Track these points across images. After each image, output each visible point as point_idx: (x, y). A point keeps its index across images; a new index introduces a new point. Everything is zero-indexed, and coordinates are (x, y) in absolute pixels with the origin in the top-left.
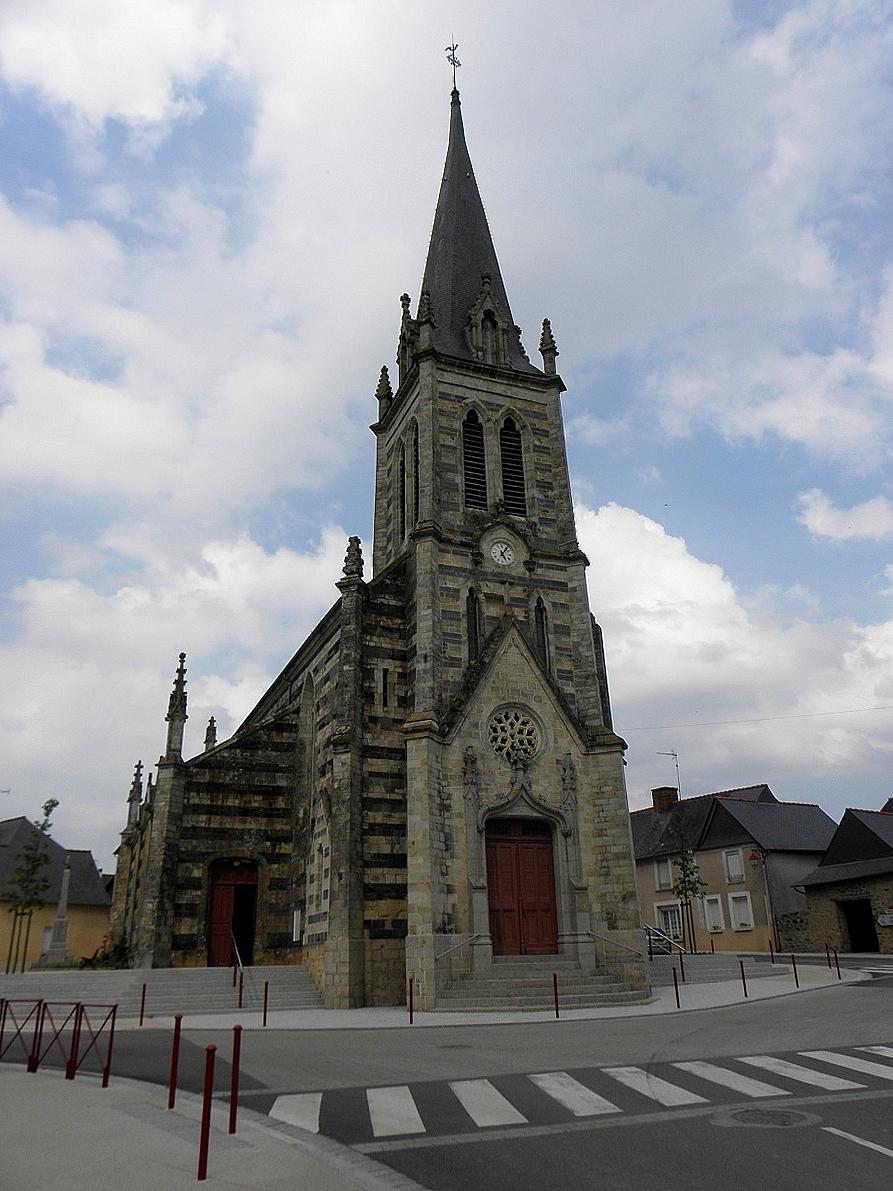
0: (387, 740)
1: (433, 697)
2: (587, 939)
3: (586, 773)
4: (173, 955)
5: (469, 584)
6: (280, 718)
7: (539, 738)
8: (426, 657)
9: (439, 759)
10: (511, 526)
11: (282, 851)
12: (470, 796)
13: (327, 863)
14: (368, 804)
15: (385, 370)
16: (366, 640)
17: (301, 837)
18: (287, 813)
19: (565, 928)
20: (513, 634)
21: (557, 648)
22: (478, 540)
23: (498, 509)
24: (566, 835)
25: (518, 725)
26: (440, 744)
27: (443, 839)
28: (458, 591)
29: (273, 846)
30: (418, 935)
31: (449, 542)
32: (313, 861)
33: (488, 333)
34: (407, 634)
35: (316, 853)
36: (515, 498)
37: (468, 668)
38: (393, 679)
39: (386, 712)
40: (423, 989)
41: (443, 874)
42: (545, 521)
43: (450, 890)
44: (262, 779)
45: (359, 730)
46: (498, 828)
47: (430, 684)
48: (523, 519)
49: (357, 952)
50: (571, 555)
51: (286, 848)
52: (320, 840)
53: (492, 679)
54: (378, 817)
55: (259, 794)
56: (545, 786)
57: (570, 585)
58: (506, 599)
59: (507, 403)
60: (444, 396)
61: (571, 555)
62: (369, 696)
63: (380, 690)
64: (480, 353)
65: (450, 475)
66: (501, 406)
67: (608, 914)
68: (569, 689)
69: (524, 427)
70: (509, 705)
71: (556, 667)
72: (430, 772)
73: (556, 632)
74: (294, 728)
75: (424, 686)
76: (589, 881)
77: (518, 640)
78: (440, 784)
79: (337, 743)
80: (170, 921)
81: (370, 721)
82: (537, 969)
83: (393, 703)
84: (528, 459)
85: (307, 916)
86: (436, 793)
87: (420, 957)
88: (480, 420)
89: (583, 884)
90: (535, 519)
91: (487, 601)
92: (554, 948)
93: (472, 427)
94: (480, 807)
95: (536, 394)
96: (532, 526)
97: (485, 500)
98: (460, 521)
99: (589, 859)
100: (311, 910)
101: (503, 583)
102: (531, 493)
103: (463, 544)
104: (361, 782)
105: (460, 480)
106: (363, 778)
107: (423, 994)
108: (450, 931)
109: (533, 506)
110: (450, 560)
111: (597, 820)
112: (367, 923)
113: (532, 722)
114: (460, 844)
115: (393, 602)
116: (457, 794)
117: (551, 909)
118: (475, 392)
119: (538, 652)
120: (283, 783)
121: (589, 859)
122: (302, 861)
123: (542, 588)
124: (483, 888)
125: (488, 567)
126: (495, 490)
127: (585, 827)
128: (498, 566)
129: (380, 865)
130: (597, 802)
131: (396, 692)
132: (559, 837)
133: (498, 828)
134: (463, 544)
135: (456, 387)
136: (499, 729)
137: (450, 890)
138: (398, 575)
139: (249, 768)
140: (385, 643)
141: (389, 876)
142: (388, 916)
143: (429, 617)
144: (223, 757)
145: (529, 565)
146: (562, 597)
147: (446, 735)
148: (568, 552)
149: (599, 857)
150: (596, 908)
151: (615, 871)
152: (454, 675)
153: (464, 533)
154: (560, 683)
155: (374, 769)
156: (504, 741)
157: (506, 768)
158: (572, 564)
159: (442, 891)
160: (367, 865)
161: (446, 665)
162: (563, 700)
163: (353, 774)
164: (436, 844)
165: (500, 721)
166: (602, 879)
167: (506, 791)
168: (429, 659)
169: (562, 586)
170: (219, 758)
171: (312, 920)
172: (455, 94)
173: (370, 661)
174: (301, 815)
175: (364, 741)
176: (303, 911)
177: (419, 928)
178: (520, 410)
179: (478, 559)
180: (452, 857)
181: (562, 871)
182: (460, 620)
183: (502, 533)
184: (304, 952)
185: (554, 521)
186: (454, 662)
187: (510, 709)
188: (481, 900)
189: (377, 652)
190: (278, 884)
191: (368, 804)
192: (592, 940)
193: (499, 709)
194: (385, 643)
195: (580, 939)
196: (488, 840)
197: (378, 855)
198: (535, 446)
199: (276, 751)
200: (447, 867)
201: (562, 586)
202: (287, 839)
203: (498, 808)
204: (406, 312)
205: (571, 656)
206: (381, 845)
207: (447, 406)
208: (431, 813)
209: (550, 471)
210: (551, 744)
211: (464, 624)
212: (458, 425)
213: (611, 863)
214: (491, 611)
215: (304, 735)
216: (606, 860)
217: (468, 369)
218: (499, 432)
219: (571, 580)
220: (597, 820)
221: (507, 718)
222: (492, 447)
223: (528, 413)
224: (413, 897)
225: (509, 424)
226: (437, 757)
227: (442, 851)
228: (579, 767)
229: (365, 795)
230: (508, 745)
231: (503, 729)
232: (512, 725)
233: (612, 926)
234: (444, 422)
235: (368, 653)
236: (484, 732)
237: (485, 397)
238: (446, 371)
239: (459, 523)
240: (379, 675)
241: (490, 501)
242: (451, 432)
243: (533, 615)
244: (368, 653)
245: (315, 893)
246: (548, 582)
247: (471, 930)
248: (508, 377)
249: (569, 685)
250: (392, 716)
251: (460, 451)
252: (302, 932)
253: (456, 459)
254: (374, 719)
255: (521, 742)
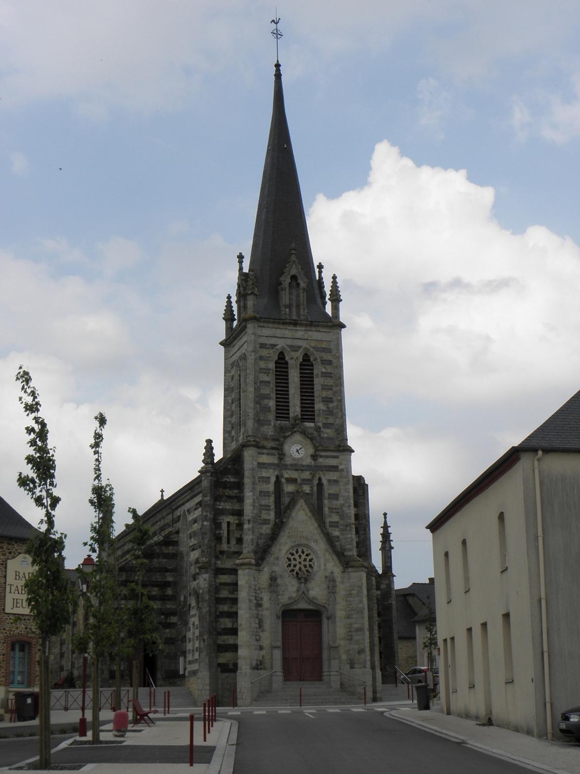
0: (228, 564)
1: (253, 545)
2: (336, 673)
3: (343, 583)
4: (111, 682)
5: (276, 473)
6: (167, 536)
7: (316, 564)
8: (249, 521)
9: (256, 579)
10: (304, 433)
11: (172, 621)
12: (273, 599)
13: (197, 633)
14: (219, 601)
15: (209, 442)
16: (217, 505)
17: (183, 613)
18: (174, 598)
19: (325, 668)
20: (301, 503)
21: (330, 508)
22: (282, 445)
23: (296, 421)
24: (328, 618)
25: (303, 557)
26: (256, 570)
27: (257, 621)
28: (269, 478)
29: (166, 618)
30: (243, 671)
31: (264, 448)
32: (190, 630)
33: (294, 291)
34: (240, 500)
35: (191, 626)
36: (308, 413)
37: (274, 525)
38: (233, 527)
39: (229, 547)
40: (245, 696)
41: (257, 640)
42: (326, 425)
43: (261, 648)
44: (158, 577)
45: (213, 559)
46: (288, 615)
47: (251, 537)
48: (312, 425)
49: (214, 680)
50: (341, 448)
51: (174, 619)
52: (193, 619)
53: (287, 531)
54: (225, 608)
55: (156, 586)
56: (317, 591)
57: (341, 467)
58: (299, 481)
59: (304, 344)
60: (263, 346)
61: (341, 448)
62: (219, 539)
63: (225, 534)
64: (287, 310)
65: (266, 401)
66: (300, 347)
67: (350, 660)
68: (336, 533)
69: (316, 359)
70: (299, 545)
71: (328, 520)
72: (250, 587)
73: (329, 498)
74: (176, 543)
75: (248, 537)
76: (342, 643)
77: (305, 506)
78: (256, 593)
79: (203, 568)
80: (108, 662)
81: (220, 554)
82: (309, 688)
83: (233, 542)
84: (318, 382)
85: (187, 660)
86: (253, 598)
87: (244, 680)
88: (287, 358)
89: (337, 645)
90: (320, 424)
91: (287, 483)
92: (319, 678)
93: (282, 363)
94: (278, 604)
95: (324, 334)
96: (318, 429)
97: (288, 414)
98: (272, 432)
99: (341, 631)
100: (190, 657)
101: (297, 470)
102: (319, 406)
103: (273, 448)
104: (216, 588)
105: (272, 404)
106: (216, 586)
107: (245, 699)
108: (261, 669)
109: (319, 415)
110: (265, 459)
111: (347, 609)
112: (219, 665)
113: (312, 554)
114: (267, 625)
115: (233, 480)
116: (266, 597)
117: (319, 659)
118: (283, 340)
119: (318, 512)
120: (170, 579)
121: (341, 631)
122: (184, 628)
123: (322, 471)
124: (278, 647)
125: (288, 461)
126: (295, 408)
127: (340, 613)
128: (294, 459)
129: (226, 634)
130: (348, 599)
131: (235, 535)
132: (325, 621)
133: (288, 615)
134: (273, 448)
135: (270, 338)
136: (292, 559)
137: (261, 648)
138: (234, 460)
139: (150, 570)
140: (228, 506)
141: (229, 640)
142: (231, 661)
143: (251, 497)
144: (132, 564)
145: (314, 457)
146: (334, 476)
147: (260, 565)
148: (339, 446)
149: (348, 630)
150: (344, 657)
151: (356, 638)
152: (266, 529)
153: (274, 440)
154: (330, 530)
155: (223, 581)
156: (295, 566)
157: (295, 582)
158: (342, 453)
159: (256, 649)
160: (219, 634)
161: (261, 524)
162: (331, 541)
163: (210, 585)
164: (253, 625)
165: (292, 554)
166: (348, 641)
167: (294, 595)
168: (251, 522)
169: (335, 468)
170: (130, 565)
171: (190, 662)
172: (278, 66)
173: (219, 518)
174: (182, 599)
175: (217, 565)
176: (185, 657)
177: (244, 667)
178: (313, 348)
179: (282, 456)
180: (263, 631)
181: (326, 638)
182: (270, 496)
183: (297, 437)
184: (187, 679)
185: (332, 424)
186: (266, 522)
187: (299, 548)
188: (278, 654)
189: (223, 512)
190: (169, 641)
191: (219, 601)
192: (338, 674)
193: (293, 547)
194: (228, 506)
195: (332, 673)
196: (283, 621)
197: (225, 629)
198: (322, 373)
199: (165, 559)
200: (260, 636)
201: (335, 468)
202: (174, 614)
203: (288, 605)
204: (241, 269)
205: (338, 512)
206: (227, 623)
207: (264, 352)
208: (250, 609)
209: (332, 389)
210: (322, 567)
211: (272, 499)
212: (272, 365)
213: (353, 633)
214: (289, 488)
215: (183, 548)
216: (351, 632)
217: (279, 323)
218: (298, 365)
219: (341, 464)
220: (347, 609)
221: (297, 552)
222: (294, 377)
223: (317, 349)
224: (241, 652)
225: (306, 358)
226: (255, 578)
227: (257, 628)
228: (338, 579)
229: (217, 596)
230: (297, 569)
231: (295, 559)
232: (300, 556)
233: (352, 667)
234: (262, 364)
235: (218, 513)
236: (283, 562)
237: (289, 342)
238: (264, 327)
239: (271, 434)
240: (224, 526)
241: (291, 415)
242: (266, 371)
243: (315, 489)
244: (218, 513)
245: (191, 648)
246: (326, 466)
247: (272, 668)
248: (306, 325)
249: (336, 531)
250: (233, 549)
251: (273, 385)
252: (185, 669)
253: (270, 390)
254: (222, 552)
255: (305, 566)
